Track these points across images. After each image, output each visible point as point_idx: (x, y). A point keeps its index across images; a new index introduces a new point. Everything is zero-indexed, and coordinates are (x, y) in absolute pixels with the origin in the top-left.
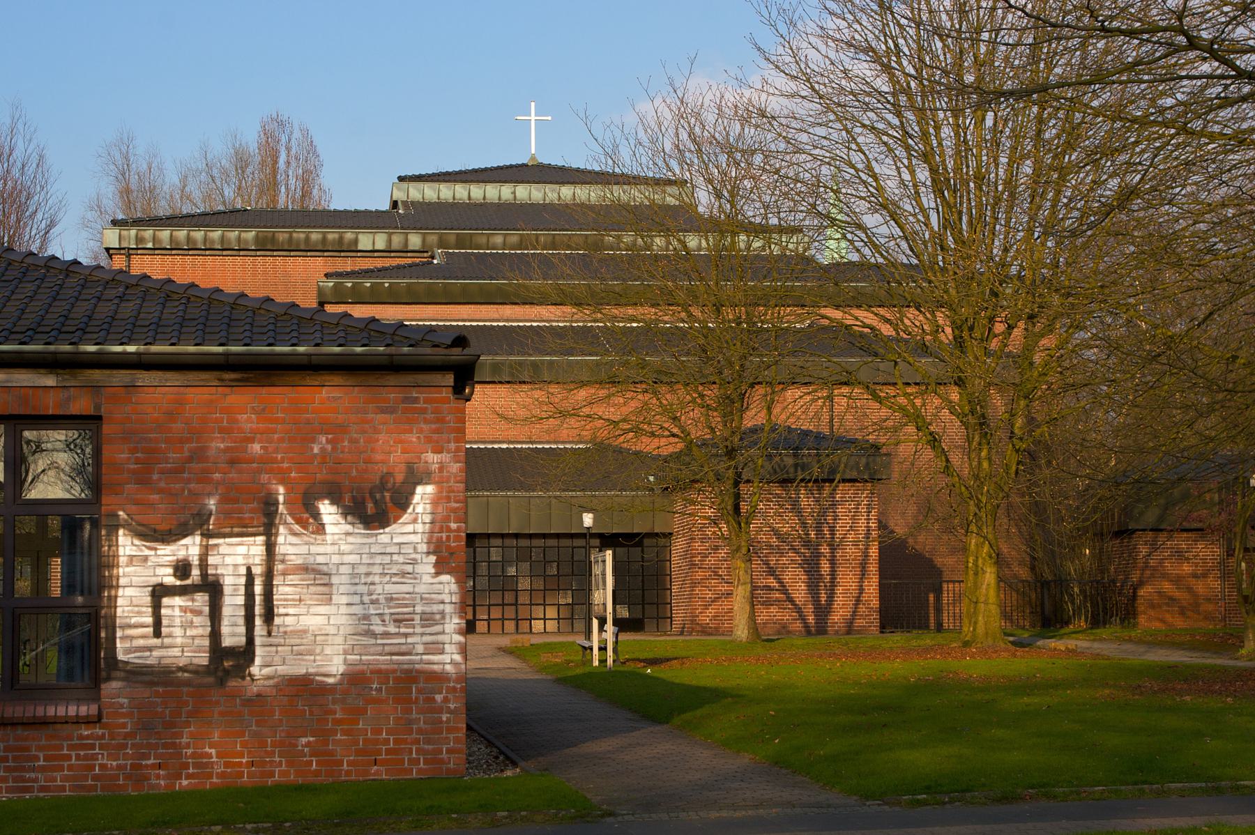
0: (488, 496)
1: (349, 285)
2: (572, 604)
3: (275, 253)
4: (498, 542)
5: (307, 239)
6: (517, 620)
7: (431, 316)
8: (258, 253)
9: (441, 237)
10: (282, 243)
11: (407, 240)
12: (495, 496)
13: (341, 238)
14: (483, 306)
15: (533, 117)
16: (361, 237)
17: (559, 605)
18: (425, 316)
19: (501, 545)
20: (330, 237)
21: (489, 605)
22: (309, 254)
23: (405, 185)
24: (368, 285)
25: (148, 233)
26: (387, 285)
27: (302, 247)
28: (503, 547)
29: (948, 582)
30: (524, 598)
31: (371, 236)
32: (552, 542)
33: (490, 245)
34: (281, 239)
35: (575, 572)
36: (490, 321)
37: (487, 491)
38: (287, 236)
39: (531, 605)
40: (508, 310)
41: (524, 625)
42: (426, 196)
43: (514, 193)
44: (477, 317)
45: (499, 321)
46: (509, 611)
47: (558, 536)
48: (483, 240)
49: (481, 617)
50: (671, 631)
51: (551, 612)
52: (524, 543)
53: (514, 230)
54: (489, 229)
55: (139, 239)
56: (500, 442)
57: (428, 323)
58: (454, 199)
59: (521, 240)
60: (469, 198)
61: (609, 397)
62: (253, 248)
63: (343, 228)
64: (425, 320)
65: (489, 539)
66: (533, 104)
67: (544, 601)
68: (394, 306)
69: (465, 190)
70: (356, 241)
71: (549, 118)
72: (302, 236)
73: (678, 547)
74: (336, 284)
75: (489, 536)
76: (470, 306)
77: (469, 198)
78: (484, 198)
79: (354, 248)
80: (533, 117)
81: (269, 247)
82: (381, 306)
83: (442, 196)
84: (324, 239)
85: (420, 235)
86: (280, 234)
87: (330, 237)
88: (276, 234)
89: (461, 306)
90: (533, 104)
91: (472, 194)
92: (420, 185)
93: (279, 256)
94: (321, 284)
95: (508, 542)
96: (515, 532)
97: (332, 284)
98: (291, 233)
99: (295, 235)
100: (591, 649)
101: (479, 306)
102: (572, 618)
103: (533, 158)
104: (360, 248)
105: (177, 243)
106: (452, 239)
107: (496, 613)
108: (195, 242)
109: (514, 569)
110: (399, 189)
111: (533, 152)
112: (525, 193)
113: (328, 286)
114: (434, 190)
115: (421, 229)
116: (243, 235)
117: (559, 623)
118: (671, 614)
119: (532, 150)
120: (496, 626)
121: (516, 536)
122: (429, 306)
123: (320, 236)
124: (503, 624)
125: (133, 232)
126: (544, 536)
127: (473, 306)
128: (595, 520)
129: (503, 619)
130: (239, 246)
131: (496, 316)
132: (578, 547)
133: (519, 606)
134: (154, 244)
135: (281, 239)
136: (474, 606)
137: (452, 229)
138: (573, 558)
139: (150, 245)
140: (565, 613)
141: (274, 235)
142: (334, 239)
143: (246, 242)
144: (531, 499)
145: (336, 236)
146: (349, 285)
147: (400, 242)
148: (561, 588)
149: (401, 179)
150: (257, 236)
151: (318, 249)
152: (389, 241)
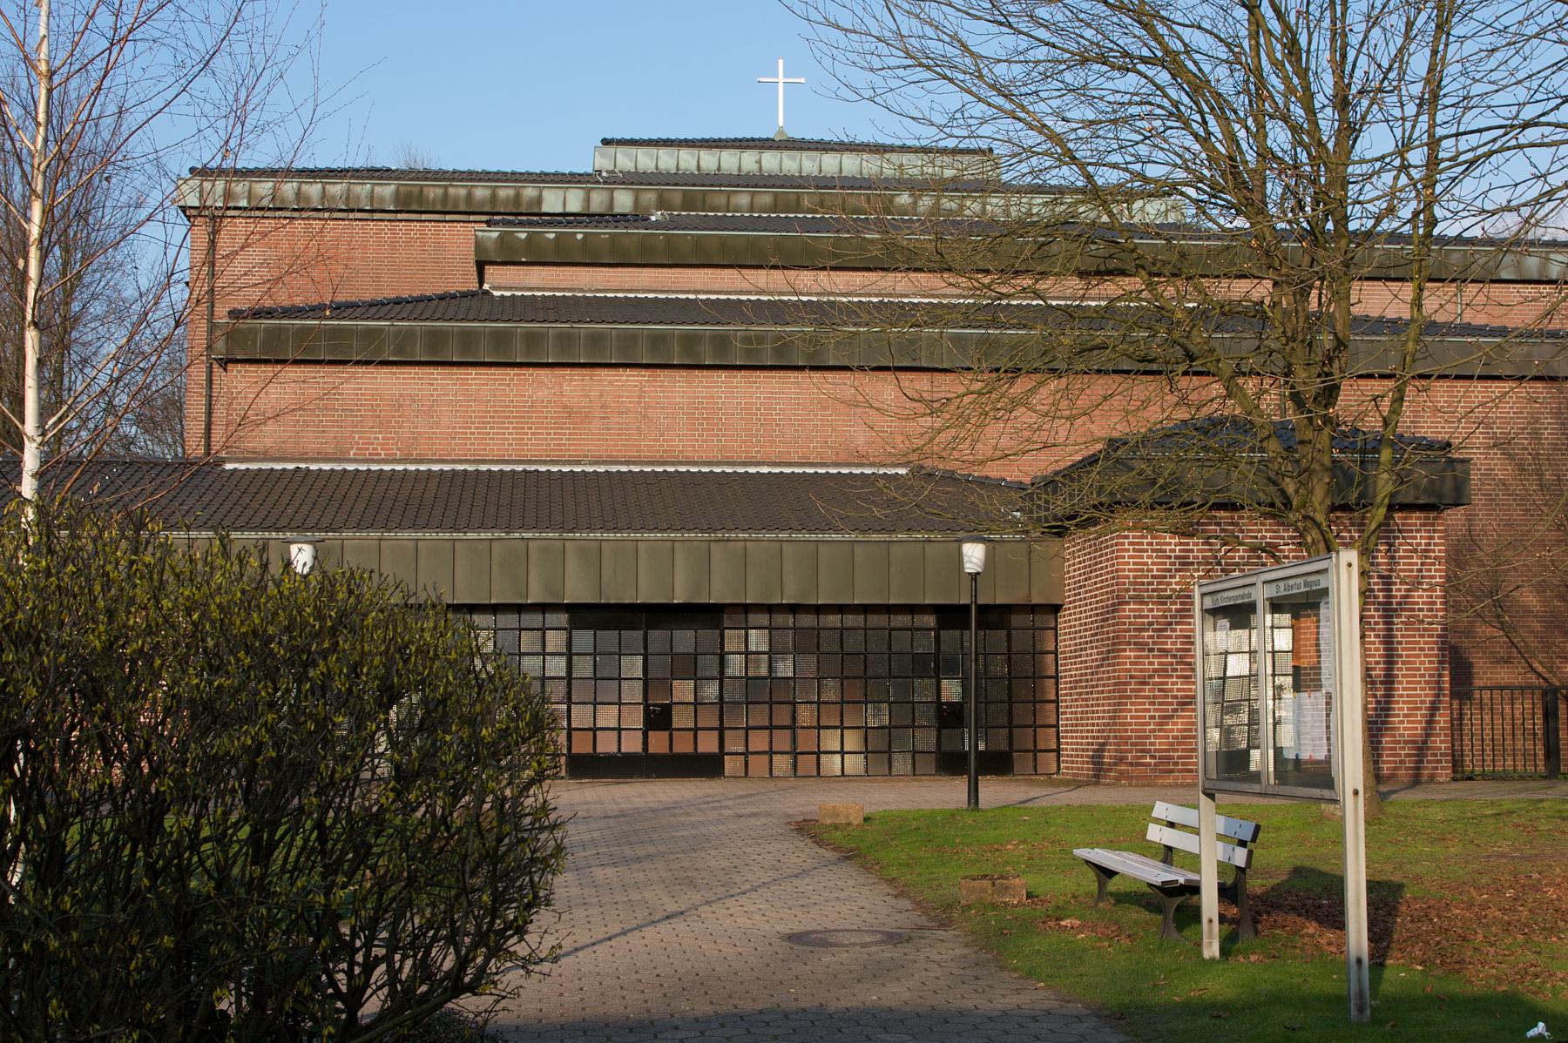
0: (745, 540)
1: (523, 236)
2: (890, 727)
3: (424, 217)
4: (763, 619)
5: (469, 196)
6: (795, 754)
7: (646, 285)
8: (400, 216)
9: (661, 195)
10: (434, 201)
11: (612, 199)
12: (758, 540)
13: (518, 196)
14: (726, 271)
15: (781, 79)
16: (546, 194)
17: (867, 728)
18: (637, 285)
19: (766, 623)
20: (502, 193)
21: (747, 729)
22: (472, 218)
23: (611, 150)
24: (552, 236)
25: (240, 188)
26: (579, 237)
27: (462, 208)
28: (770, 628)
29: (1481, 689)
30: (805, 715)
31: (561, 192)
32: (852, 620)
33: (731, 208)
34: (432, 196)
35: (895, 673)
36: (736, 293)
37: (744, 531)
38: (440, 191)
39: (819, 727)
40: (761, 278)
41: (806, 763)
42: (639, 167)
43: (759, 162)
44: (717, 287)
45: (749, 293)
46: (782, 740)
47: (865, 609)
48: (722, 200)
49: (734, 749)
50: (1058, 772)
51: (853, 741)
52: (807, 620)
53: (765, 186)
54: (729, 186)
55: (228, 195)
56: (758, 464)
57: (643, 296)
58: (678, 169)
59: (776, 200)
60: (699, 168)
61: (1130, 196)
62: (392, 208)
63: (521, 181)
64: (638, 291)
65: (746, 613)
66: (781, 62)
67: (842, 721)
68: (591, 269)
69: (693, 157)
70: (539, 200)
71: (803, 80)
72: (463, 192)
73: (1073, 629)
74: (502, 236)
75: (746, 608)
76: (706, 270)
77: (699, 168)
78: (719, 169)
79: (535, 210)
80: (781, 79)
81: (414, 207)
82: (572, 269)
83: (662, 166)
84: (494, 197)
85: (631, 193)
86: (431, 189)
87: (502, 193)
88: (426, 190)
89: (693, 270)
90: (781, 62)
91: (701, 163)
92: (633, 150)
93: (430, 221)
94: (480, 234)
95: (780, 619)
96: (793, 602)
97: (496, 234)
98: (446, 187)
99: (452, 191)
100: (1193, 889)
101: (719, 271)
102: (889, 752)
103: (781, 131)
104: (545, 209)
105: (283, 201)
106: (677, 198)
107: (759, 741)
108: (308, 199)
109: (790, 663)
110: (603, 155)
111: (781, 124)
112: (771, 162)
113: (490, 237)
114: (652, 158)
115: (632, 183)
116: (378, 189)
117: (866, 758)
118: (1059, 743)
119: (780, 122)
120: (758, 764)
121: (794, 609)
122: (645, 270)
123: (487, 192)
124: (771, 761)
125: (220, 185)
126: (841, 609)
127: (710, 271)
128: (990, 559)
129: (771, 753)
130: (372, 205)
131: (745, 286)
132: (900, 629)
133: (799, 732)
134: (249, 202)
135: (432, 196)
136: (721, 730)
137: (676, 185)
138: (890, 648)
139: (243, 203)
140: (877, 742)
141: (421, 191)
142: (508, 198)
143: (382, 199)
144: (820, 545)
145: (511, 192)
146: (523, 236)
147: (602, 202)
148: (869, 699)
149: (606, 142)
150: (397, 190)
151: (485, 210)
152: (587, 200)
